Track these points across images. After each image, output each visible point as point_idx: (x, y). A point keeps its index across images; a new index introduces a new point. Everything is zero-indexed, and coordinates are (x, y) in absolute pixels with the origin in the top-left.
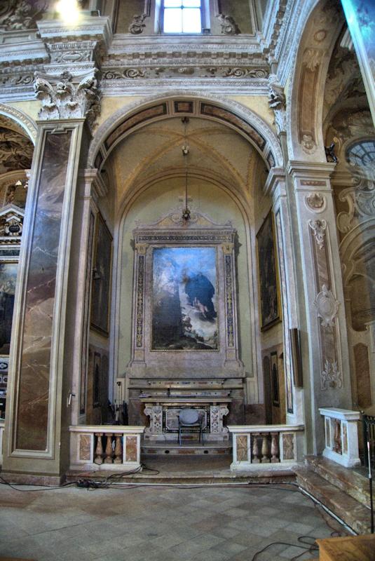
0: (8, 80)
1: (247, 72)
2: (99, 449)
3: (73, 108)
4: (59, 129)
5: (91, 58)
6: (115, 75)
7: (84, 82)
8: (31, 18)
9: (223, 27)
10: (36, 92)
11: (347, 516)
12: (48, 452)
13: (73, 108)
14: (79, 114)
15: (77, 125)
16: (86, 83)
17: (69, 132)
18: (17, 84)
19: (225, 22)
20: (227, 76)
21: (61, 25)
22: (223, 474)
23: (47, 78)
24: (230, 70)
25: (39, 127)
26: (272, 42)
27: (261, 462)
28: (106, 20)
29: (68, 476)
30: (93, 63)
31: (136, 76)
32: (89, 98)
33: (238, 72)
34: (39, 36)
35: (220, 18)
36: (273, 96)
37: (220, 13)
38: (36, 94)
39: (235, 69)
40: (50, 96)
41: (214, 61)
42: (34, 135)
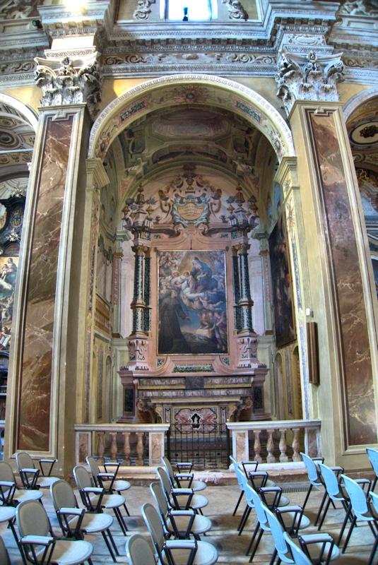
4: (61, 116)
11: (280, 275)
12: (51, 453)
16: (88, 67)
17: (70, 119)
18: (16, 71)
20: (233, 61)
21: (66, 10)
31: (138, 62)
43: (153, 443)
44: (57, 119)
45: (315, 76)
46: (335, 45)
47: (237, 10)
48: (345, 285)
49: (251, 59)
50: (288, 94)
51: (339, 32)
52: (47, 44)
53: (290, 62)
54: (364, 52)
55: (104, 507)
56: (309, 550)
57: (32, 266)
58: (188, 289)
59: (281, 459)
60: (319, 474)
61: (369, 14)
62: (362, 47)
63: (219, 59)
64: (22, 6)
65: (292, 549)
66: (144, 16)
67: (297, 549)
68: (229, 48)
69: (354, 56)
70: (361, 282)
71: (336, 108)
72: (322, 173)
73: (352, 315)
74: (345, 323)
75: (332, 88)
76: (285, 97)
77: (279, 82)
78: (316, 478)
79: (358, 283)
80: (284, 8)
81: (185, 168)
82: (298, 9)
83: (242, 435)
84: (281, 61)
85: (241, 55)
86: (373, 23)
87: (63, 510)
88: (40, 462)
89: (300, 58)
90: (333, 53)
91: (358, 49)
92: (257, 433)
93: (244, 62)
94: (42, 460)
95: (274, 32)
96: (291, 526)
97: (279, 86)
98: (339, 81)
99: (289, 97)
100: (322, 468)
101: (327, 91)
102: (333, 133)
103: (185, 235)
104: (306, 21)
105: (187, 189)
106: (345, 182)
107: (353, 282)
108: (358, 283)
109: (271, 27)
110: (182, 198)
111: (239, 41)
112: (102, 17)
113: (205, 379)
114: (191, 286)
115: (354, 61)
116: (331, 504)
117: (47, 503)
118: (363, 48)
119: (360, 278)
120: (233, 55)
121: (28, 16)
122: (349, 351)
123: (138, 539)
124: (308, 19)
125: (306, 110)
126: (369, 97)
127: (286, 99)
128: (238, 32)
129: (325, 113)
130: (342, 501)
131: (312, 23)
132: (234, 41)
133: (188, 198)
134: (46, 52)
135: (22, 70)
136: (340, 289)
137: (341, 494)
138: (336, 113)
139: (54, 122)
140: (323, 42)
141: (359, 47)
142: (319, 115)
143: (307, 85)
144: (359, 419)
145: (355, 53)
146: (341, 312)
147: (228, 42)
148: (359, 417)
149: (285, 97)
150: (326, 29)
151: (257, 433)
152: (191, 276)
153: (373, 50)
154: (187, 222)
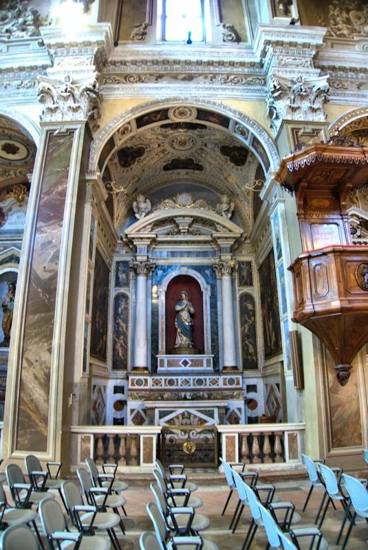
0: (214, 77)
1: (244, 80)
2: (245, 449)
3: (75, 110)
5: (92, 62)
6: (116, 81)
9: (224, 35)
10: (39, 95)
12: (49, 454)
13: (75, 110)
14: (82, 116)
17: (71, 133)
19: (226, 30)
20: (225, 83)
23: (49, 81)
24: (228, 78)
25: (42, 129)
26: (265, 47)
27: (274, 461)
28: (107, 27)
32: (90, 101)
33: (236, 79)
34: (42, 44)
35: (221, 27)
36: (275, 87)
37: (221, 21)
38: (39, 98)
39: (232, 77)
41: (217, 69)
42: (39, 140)
44: (59, 133)
46: (323, 68)
47: (230, 33)
49: (242, 81)
52: (49, 63)
53: (279, 84)
55: (108, 506)
56: (300, 543)
57: (333, 419)
59: (254, 461)
60: (319, 475)
63: (211, 80)
64: (25, 27)
65: (283, 540)
66: (141, 37)
67: (288, 542)
69: (338, 77)
71: (323, 128)
75: (319, 109)
76: (274, 116)
77: (268, 102)
78: (317, 478)
83: (86, 440)
84: (271, 85)
86: (29, 44)
87: (16, 485)
88: (48, 465)
90: (320, 75)
94: (49, 463)
95: (264, 53)
96: (282, 521)
97: (268, 105)
98: (326, 101)
99: (277, 117)
100: (322, 469)
101: (314, 110)
112: (102, 38)
116: (331, 502)
117: (118, 531)
121: (31, 36)
123: (48, 503)
125: (293, 129)
127: (275, 119)
129: (314, 133)
130: (341, 500)
134: (48, 70)
135: (24, 87)
137: (340, 493)
138: (322, 132)
139: (55, 136)
142: (305, 134)
143: (295, 105)
149: (274, 116)
150: (314, 53)
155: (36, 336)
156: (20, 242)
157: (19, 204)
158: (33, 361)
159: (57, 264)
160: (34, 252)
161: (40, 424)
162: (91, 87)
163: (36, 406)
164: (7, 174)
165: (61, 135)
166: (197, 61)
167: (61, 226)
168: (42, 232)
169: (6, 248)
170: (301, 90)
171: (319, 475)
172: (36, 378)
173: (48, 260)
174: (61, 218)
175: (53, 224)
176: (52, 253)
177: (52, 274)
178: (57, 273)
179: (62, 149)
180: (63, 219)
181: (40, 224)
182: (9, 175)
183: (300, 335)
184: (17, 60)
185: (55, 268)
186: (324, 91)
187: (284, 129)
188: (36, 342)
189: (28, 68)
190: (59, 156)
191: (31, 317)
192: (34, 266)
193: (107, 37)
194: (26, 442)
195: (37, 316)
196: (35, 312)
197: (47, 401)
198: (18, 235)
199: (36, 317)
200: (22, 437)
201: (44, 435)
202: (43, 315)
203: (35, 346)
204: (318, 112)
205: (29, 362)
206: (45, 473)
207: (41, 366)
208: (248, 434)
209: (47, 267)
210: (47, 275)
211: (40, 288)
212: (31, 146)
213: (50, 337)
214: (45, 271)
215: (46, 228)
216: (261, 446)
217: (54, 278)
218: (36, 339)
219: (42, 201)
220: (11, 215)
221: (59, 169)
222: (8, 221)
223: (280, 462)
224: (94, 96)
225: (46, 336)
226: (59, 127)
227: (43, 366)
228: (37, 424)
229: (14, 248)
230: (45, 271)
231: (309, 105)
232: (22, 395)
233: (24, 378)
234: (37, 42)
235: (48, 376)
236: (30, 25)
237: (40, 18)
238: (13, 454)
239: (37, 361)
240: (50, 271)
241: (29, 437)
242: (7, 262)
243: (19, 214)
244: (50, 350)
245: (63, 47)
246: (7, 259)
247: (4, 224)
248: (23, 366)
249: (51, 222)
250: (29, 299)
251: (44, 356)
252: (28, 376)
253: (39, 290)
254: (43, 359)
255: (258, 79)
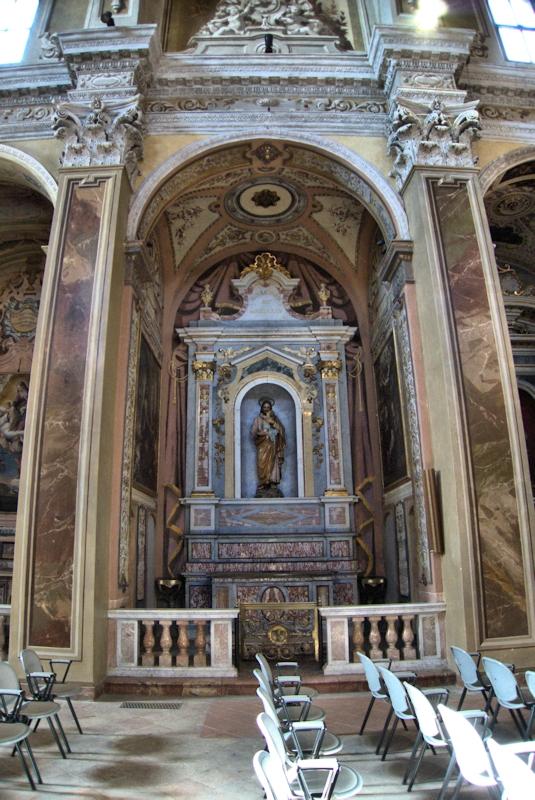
1: (354, 106)
3: (107, 151)
7: (123, 113)
8: (155, 25)
10: (55, 129)
14: (116, 159)
15: (113, 174)
22: (315, 681)
26: (384, 59)
29: (110, 689)
30: (135, 89)
38: (56, 133)
40: (77, 134)
42: (53, 191)
43: (332, 643)
45: (441, 134)
48: (55, 423)
50: (402, 157)
51: (174, 63)
54: (212, 87)
58: (7, 425)
60: (382, 681)
61: (242, 32)
62: (207, 80)
63: (6, 118)
68: (23, 100)
70: (80, 420)
72: (64, 267)
73: (58, 465)
74: (47, 476)
75: (465, 149)
76: (398, 160)
79: (76, 420)
80: (78, 40)
81: (29, 262)
82: (97, 39)
85: (37, 109)
86: (243, 46)
88: (51, 663)
89: (83, 108)
91: (202, 84)
92: (149, 625)
93: (38, 119)
97: (390, 142)
98: (475, 138)
101: (458, 152)
102: (96, 209)
103: (14, 352)
104: (108, 55)
105: (28, 289)
106: (92, 278)
107: (70, 419)
108: (76, 420)
109: (380, 61)
110: (18, 302)
111: (34, 90)
113: (5, 546)
114: (11, 421)
115: (194, 101)
118: (210, 83)
119: (80, 414)
120: (27, 110)
122: (45, 515)
124: (109, 52)
125: (427, 179)
126: (200, 152)
128: (33, 78)
129: (455, 183)
131: (116, 57)
132: (28, 92)
133: (25, 302)
135: (335, 108)
136: (47, 428)
138: (110, 181)
140: (129, 82)
141: (202, 81)
142: (87, 186)
143: (430, 143)
144: (47, 611)
145: (198, 91)
146: (43, 460)
147: (21, 93)
148: (47, 608)
150: (455, 66)
151: (149, 625)
152: (12, 408)
153: (224, 83)
154: (19, 334)
155: (491, 474)
156: (519, 338)
157: (262, 282)
158: (492, 509)
159: (497, 371)
160: (462, 355)
161: (515, 597)
162: (131, 119)
163: (507, 573)
164: (240, 237)
165: (449, 187)
166: (290, 78)
167: (489, 317)
168: (465, 325)
169: (254, 349)
170: (440, 121)
171: (382, 681)
172: (501, 533)
173: (484, 366)
174: (486, 307)
175: (477, 314)
176: (487, 355)
177: (493, 385)
178: (500, 384)
179: (458, 207)
180: (488, 308)
181: (459, 314)
182: (244, 238)
183: (439, 473)
184: (322, 68)
185: (495, 378)
186: (472, 124)
187: (415, 178)
188: (492, 482)
189: (340, 81)
190: (456, 217)
191: (478, 446)
192: (468, 375)
193: (152, 43)
194: (499, 624)
195: (486, 446)
196: (482, 441)
197: (520, 563)
198: (269, 329)
199: (485, 447)
200: (492, 619)
201: (521, 611)
202: (494, 443)
203: (492, 488)
204: (465, 154)
205: (489, 513)
206: (48, 674)
207: (504, 514)
208: (380, 619)
209: (485, 375)
210: (488, 387)
211: (483, 405)
212: (40, 200)
213: (508, 474)
214: (483, 381)
215: (468, 320)
216: (366, 633)
217: (498, 389)
218: (492, 478)
219: (453, 282)
220: (253, 299)
221: (462, 236)
222: (249, 308)
223: (201, 665)
224: (135, 129)
225: (502, 474)
226: (441, 175)
227: (508, 514)
228: (510, 598)
229: (269, 348)
230: (483, 381)
231: (451, 143)
232: (485, 558)
233: (483, 534)
234: (333, 43)
235: (516, 529)
236: (310, 17)
237: (323, 8)
238: (483, 645)
239: (498, 509)
240: (491, 382)
241: (502, 617)
242: (258, 370)
243: (264, 297)
244: (513, 493)
245: (409, 57)
246: (259, 365)
247: (244, 312)
248: (480, 517)
249: (474, 312)
250: (471, 421)
251: (507, 501)
252: (488, 531)
253: (482, 408)
254: (506, 506)
255: (375, 104)
